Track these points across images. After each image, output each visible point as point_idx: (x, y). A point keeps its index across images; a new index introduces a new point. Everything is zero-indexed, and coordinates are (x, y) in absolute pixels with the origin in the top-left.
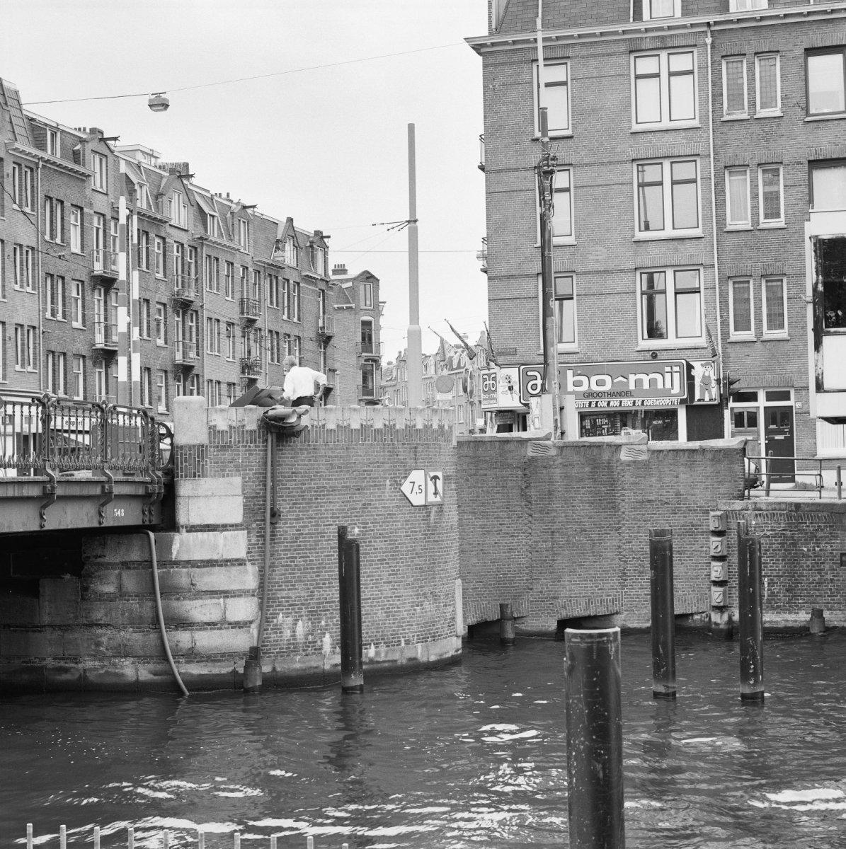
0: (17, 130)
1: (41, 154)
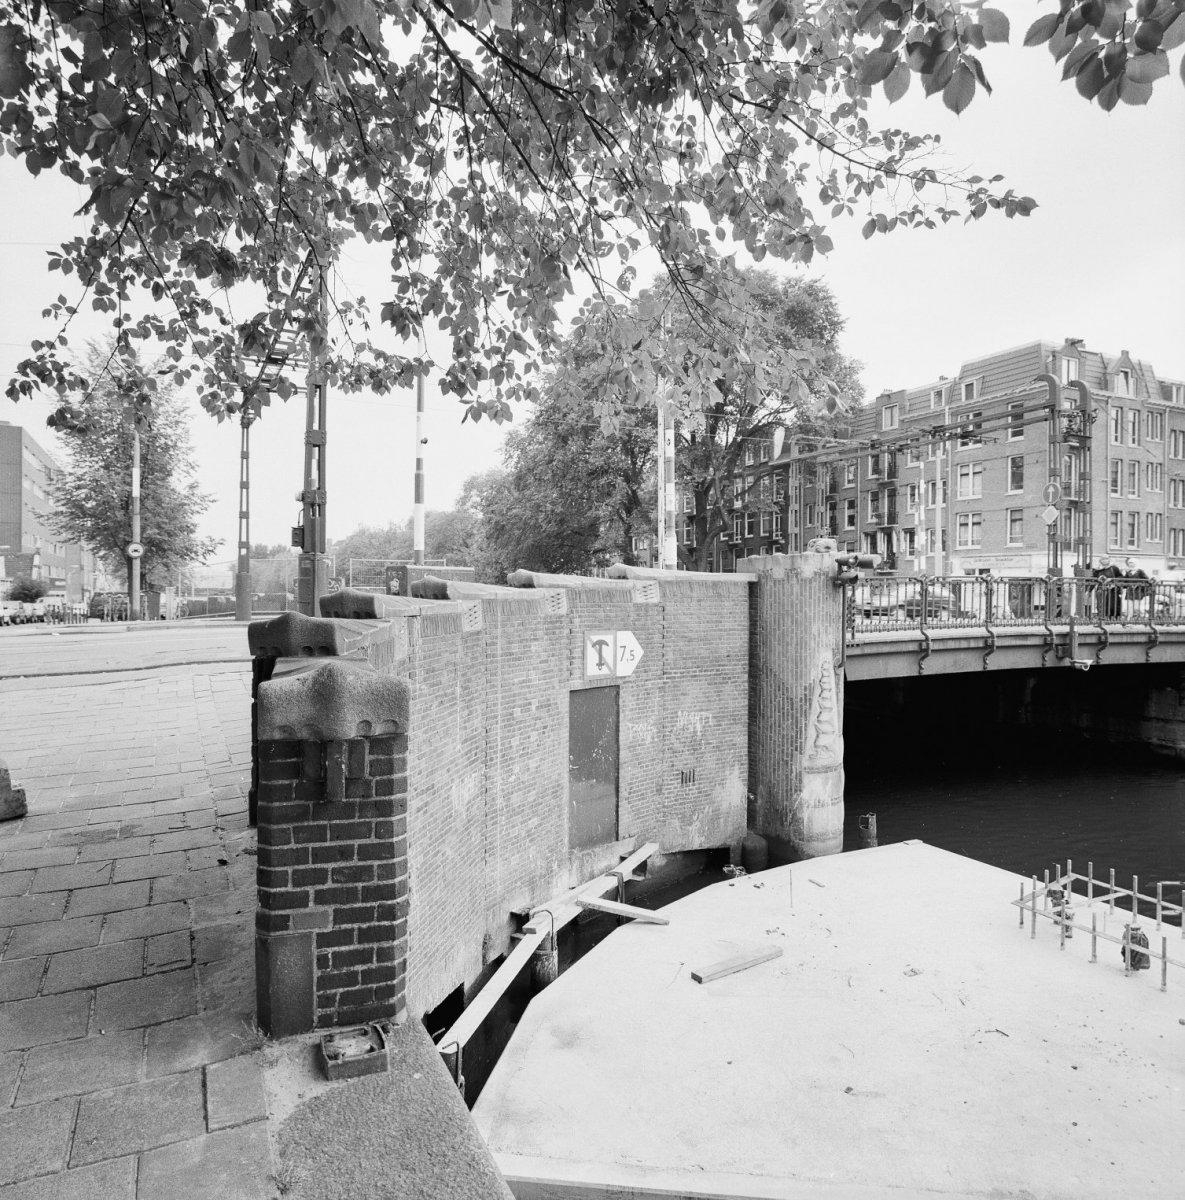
0: (1150, 390)
1: (1168, 403)
